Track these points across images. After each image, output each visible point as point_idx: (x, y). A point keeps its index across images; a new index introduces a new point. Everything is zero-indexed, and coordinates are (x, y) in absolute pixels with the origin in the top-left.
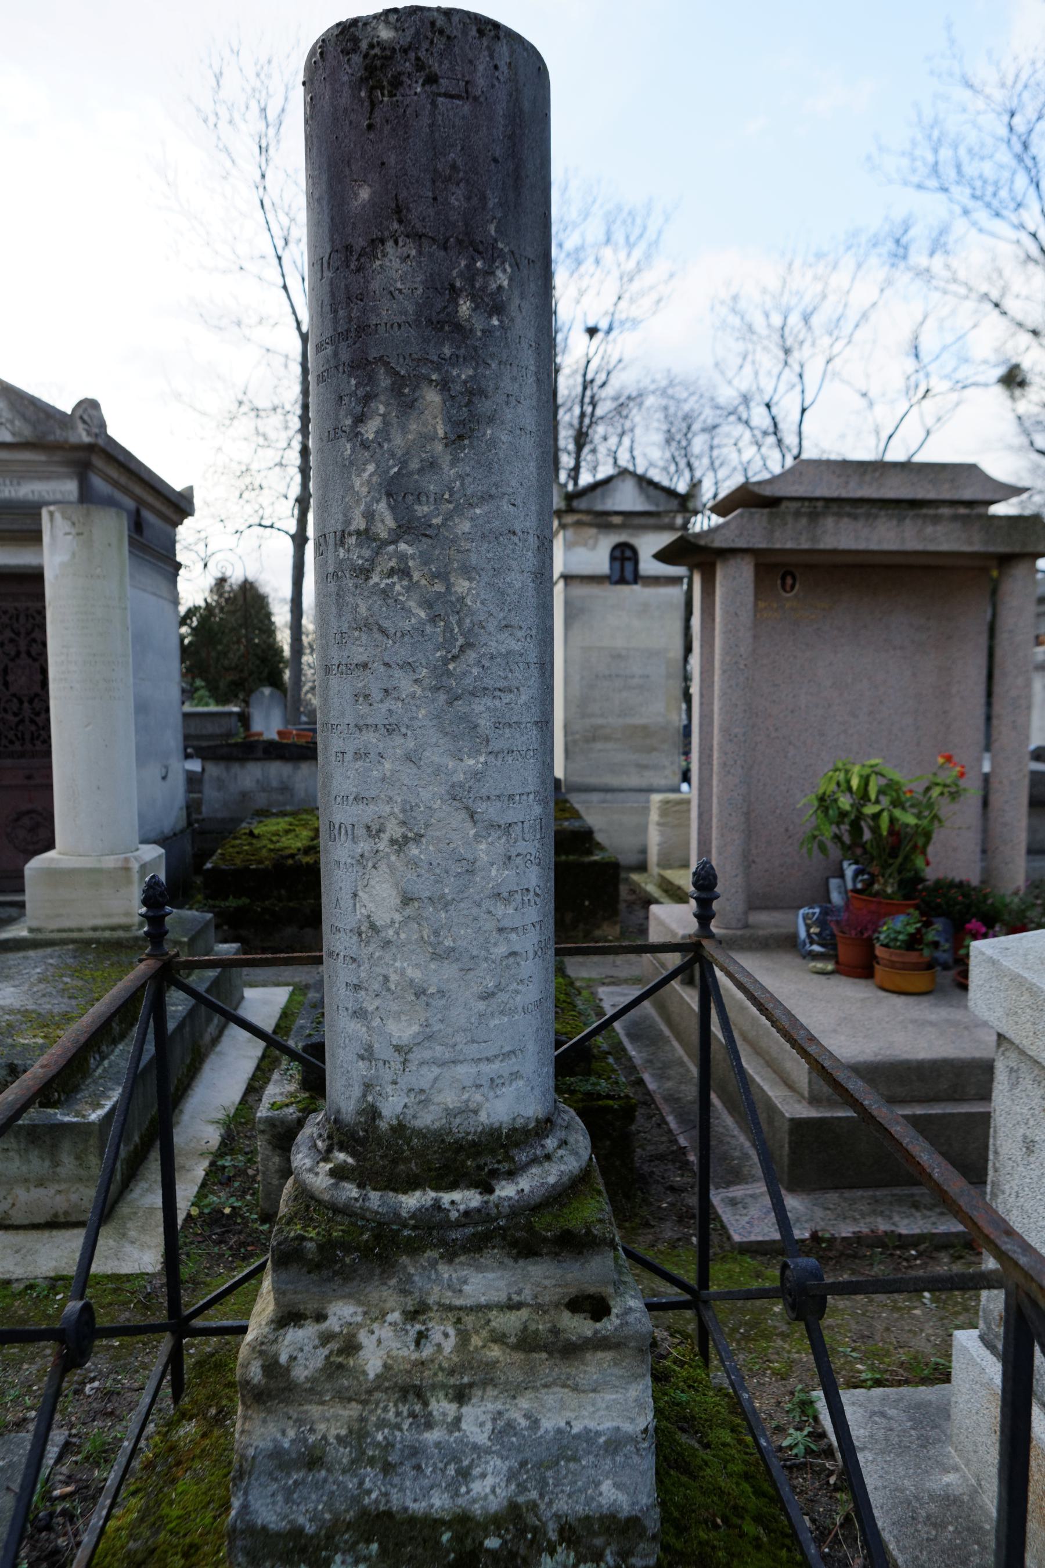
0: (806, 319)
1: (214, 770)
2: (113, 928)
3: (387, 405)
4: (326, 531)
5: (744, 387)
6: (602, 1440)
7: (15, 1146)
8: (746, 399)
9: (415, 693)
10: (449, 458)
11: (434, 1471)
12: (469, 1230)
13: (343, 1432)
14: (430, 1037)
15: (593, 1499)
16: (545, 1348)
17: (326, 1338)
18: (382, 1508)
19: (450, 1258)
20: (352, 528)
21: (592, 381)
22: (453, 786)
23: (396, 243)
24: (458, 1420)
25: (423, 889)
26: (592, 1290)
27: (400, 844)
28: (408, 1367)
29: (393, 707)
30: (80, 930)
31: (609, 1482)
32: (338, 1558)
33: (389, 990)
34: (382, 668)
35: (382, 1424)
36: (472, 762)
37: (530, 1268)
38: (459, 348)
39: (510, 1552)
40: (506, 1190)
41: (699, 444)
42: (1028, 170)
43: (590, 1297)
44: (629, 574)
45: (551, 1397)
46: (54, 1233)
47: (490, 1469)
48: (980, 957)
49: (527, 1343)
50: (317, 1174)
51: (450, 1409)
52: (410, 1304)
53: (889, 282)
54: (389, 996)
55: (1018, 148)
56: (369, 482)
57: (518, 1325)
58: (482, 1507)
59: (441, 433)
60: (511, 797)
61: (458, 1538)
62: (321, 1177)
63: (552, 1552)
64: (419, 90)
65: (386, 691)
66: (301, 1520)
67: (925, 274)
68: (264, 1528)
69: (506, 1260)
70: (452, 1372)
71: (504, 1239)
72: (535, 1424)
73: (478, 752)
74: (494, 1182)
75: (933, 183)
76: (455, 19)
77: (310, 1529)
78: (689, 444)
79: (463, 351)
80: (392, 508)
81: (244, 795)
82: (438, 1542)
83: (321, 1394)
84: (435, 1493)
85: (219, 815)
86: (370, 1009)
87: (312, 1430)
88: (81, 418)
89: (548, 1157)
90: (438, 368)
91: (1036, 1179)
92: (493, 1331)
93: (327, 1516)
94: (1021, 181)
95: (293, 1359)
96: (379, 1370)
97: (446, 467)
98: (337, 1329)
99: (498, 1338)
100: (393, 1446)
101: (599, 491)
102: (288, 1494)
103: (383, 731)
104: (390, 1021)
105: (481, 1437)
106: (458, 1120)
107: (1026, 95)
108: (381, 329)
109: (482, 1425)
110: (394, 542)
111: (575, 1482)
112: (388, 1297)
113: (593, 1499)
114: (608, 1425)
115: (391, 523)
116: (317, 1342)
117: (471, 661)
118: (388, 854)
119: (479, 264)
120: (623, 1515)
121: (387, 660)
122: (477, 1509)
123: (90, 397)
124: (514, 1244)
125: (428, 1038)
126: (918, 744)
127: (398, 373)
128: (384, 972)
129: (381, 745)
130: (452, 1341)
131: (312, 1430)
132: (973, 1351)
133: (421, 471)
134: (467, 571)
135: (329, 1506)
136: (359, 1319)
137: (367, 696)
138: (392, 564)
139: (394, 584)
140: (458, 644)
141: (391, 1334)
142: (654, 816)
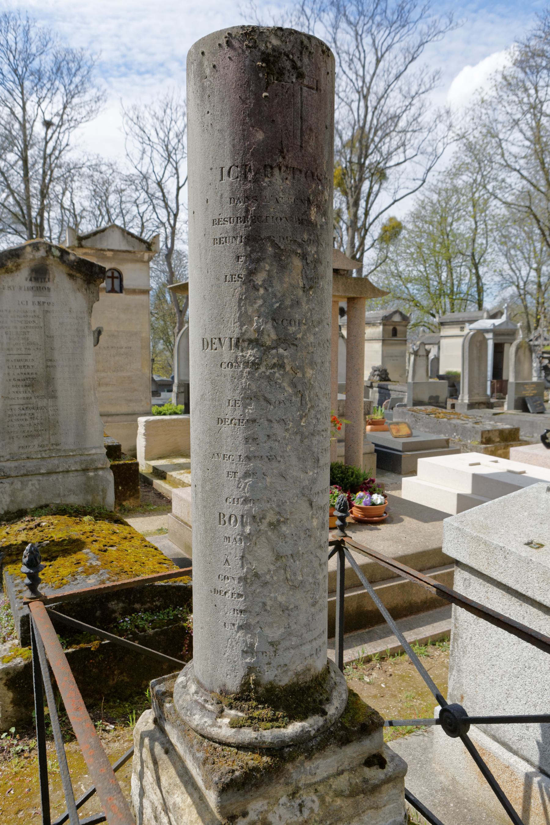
3: (271, 265)
4: (221, 336)
9: (285, 436)
10: (305, 299)
12: (318, 739)
14: (290, 634)
16: (363, 792)
19: (309, 757)
20: (246, 337)
21: (50, 155)
23: (280, 169)
25: (287, 550)
33: (266, 610)
34: (266, 423)
36: (311, 473)
38: (310, 235)
41: (113, 199)
43: (374, 756)
44: (117, 288)
49: (354, 792)
52: (290, 789)
54: (266, 614)
56: (258, 311)
59: (301, 285)
64: (294, 80)
65: (268, 436)
69: (336, 749)
71: (335, 738)
74: (323, 707)
78: (107, 198)
80: (275, 328)
86: (253, 623)
90: (300, 245)
91: (483, 631)
98: (256, 818)
99: (339, 794)
101: (98, 236)
106: (302, 677)
112: (280, 791)
115: (274, 336)
118: (266, 532)
121: (270, 417)
125: (289, 634)
127: (280, 247)
129: (264, 468)
130: (317, 803)
133: (292, 306)
134: (312, 364)
136: (266, 807)
137: (254, 439)
138: (275, 361)
139: (275, 373)
141: (285, 811)
142: (141, 430)
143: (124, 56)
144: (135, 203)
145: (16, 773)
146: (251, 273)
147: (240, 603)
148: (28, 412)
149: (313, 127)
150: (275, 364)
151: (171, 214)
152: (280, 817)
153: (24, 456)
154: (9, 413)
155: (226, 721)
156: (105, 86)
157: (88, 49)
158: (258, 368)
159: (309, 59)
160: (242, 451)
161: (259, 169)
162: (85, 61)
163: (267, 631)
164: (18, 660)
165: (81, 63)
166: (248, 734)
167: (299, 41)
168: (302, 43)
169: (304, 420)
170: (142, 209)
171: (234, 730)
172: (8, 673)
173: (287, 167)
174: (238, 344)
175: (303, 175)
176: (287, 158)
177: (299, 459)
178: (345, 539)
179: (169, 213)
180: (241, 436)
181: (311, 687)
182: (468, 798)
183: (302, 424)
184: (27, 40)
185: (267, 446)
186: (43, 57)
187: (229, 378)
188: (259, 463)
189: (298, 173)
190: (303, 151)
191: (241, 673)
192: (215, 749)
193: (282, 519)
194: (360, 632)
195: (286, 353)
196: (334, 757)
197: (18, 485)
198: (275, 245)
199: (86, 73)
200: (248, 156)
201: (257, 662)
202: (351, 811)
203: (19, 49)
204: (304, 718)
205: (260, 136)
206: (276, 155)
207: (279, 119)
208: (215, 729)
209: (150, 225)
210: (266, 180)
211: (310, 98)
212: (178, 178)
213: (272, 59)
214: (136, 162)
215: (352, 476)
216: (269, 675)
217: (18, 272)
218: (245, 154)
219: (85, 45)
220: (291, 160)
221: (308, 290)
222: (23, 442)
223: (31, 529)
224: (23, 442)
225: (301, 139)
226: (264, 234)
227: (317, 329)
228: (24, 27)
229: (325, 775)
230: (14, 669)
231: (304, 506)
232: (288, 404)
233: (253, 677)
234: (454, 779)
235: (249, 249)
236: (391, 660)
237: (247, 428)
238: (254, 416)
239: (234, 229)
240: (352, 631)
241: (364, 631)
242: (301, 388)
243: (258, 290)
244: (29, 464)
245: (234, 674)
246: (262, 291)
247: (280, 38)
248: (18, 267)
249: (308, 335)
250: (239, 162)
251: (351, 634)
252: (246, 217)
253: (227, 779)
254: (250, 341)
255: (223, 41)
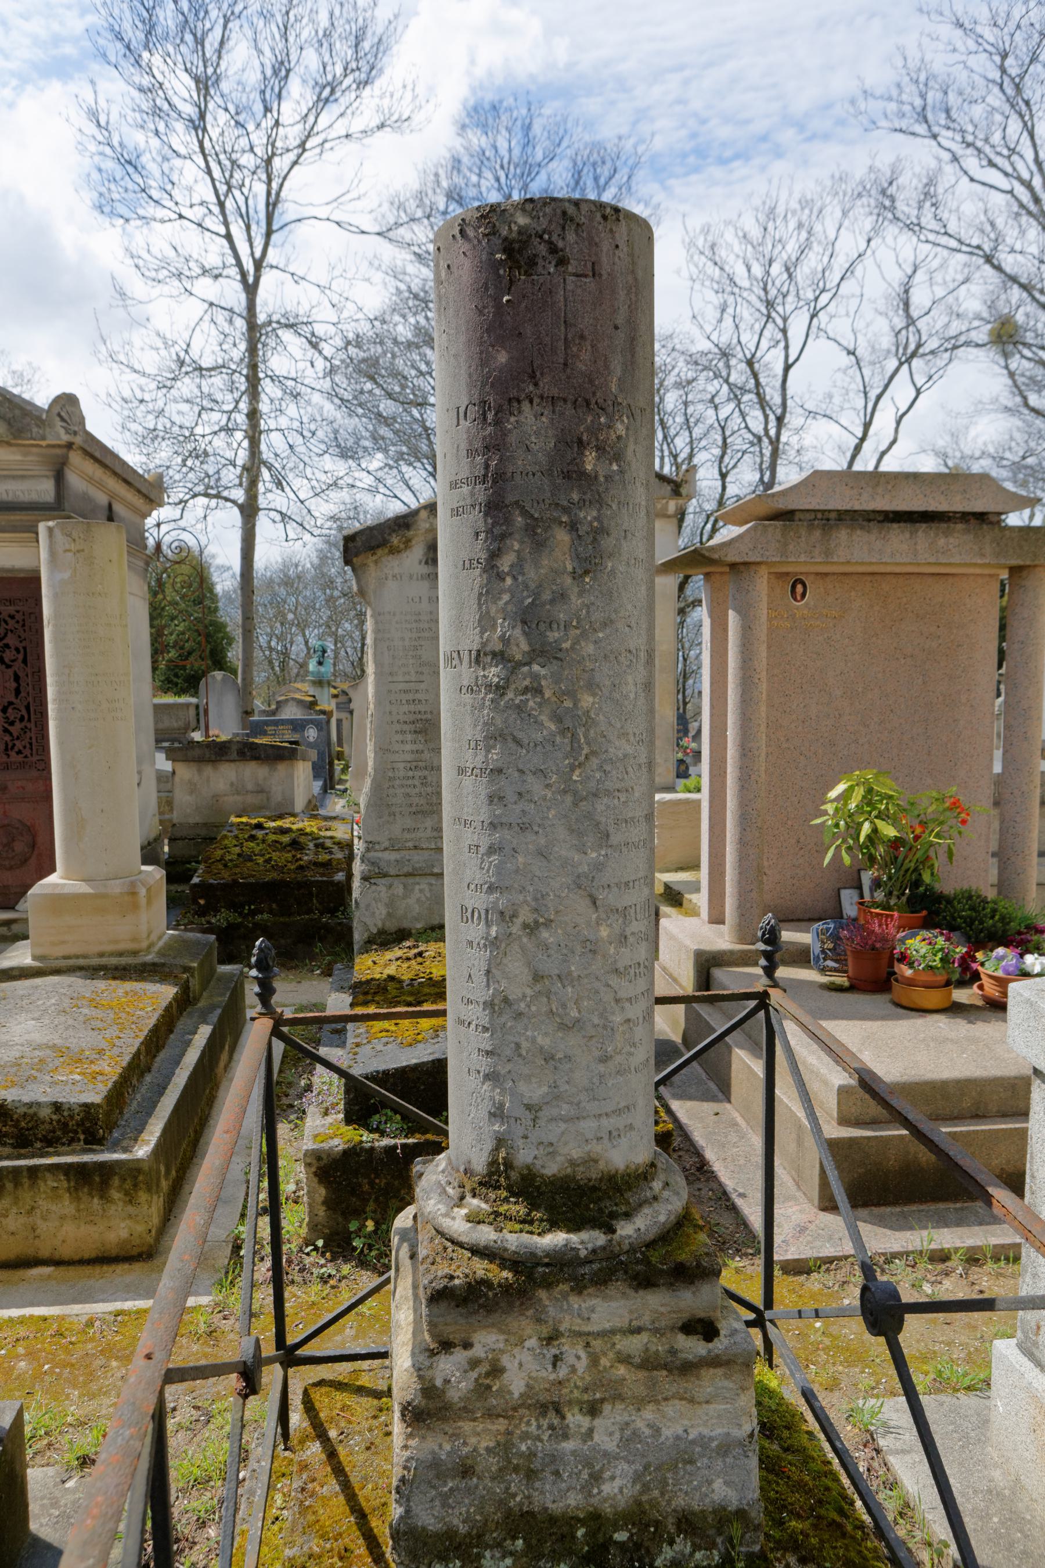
0: (789, 272)
1: (185, 772)
2: (121, 954)
3: (522, 542)
4: (460, 648)
5: (724, 340)
6: (714, 1444)
7: (65, 1184)
8: (725, 355)
10: (576, 590)
11: (570, 1476)
12: (596, 1266)
13: (492, 1444)
14: (557, 1097)
15: (706, 1495)
16: (665, 1366)
17: (474, 1363)
18: (525, 1509)
19: (579, 1289)
20: (488, 649)
22: (578, 877)
23: (531, 402)
24: (591, 1430)
25: (550, 966)
26: (702, 1315)
27: (531, 928)
28: (547, 1386)
29: (527, 809)
30: (85, 957)
31: (721, 1480)
32: (488, 1554)
33: (520, 1055)
34: (516, 774)
35: (525, 1437)
36: (594, 855)
37: (649, 1297)
38: (584, 493)
39: (635, 1544)
40: (626, 1230)
42: (1021, 116)
43: (701, 1321)
45: (671, 1409)
46: (105, 1268)
47: (618, 1473)
48: (1018, 998)
49: (648, 1363)
50: (454, 1218)
51: (585, 1421)
52: (545, 1331)
53: (876, 230)
54: (521, 1061)
55: (1010, 91)
56: (504, 610)
57: (640, 1346)
58: (611, 1506)
59: (570, 568)
60: (627, 884)
61: (591, 1534)
62: (457, 1221)
63: (671, 1543)
64: (552, 270)
66: (456, 1521)
67: (914, 227)
68: (424, 1529)
69: (628, 1291)
70: (586, 1390)
71: (626, 1272)
72: (657, 1431)
73: (601, 847)
74: (614, 1222)
75: (921, 129)
76: (584, 208)
77: (463, 1529)
79: (588, 497)
80: (524, 633)
81: (216, 797)
82: (574, 1537)
83: (473, 1412)
84: (571, 1495)
85: (191, 821)
86: (503, 1072)
87: (465, 1443)
88: (59, 415)
89: (655, 1198)
90: (566, 510)
92: (619, 1352)
93: (478, 1518)
94: (1015, 126)
95: (447, 1381)
96: (522, 1389)
97: (573, 598)
98: (483, 1355)
99: (624, 1359)
100: (535, 1455)
102: (444, 1498)
103: (517, 829)
104: (521, 1083)
105: (610, 1445)
106: (582, 1169)
107: (1019, 37)
108: (517, 477)
109: (611, 1434)
110: (528, 664)
111: (691, 1482)
112: (524, 1325)
113: (706, 1495)
114: (719, 1431)
115: (525, 647)
116: (467, 1367)
117: (595, 767)
119: (602, 420)
120: (732, 1508)
121: (521, 767)
122: (607, 1509)
123: (68, 391)
124: (635, 1277)
125: (556, 1096)
126: (929, 754)
127: (532, 516)
128: (516, 1040)
131: (465, 1443)
132: (1012, 1358)
133: (552, 602)
134: (592, 687)
135: (480, 1509)
136: (501, 1345)
137: (501, 798)
138: (527, 682)
140: (584, 752)
143: (694, 136)
144: (713, 402)
145: (313, 1303)
146: (494, 555)
147: (485, 1041)
148: (418, 774)
149: (586, 333)
150: (526, 688)
151: (772, 417)
152: (521, 1365)
153: (410, 844)
154: (390, 774)
155: (464, 1211)
156: (659, 197)
157: (630, 136)
158: (503, 694)
159: (577, 234)
160: (484, 815)
161: (501, 406)
162: (623, 158)
163: (523, 1087)
164: (336, 1141)
165: (618, 164)
166: (486, 1235)
167: (559, 211)
168: (564, 213)
169: (577, 772)
170: (724, 413)
171: (469, 1225)
172: (319, 1159)
173: (542, 397)
174: (478, 658)
175: (569, 405)
176: (541, 384)
177: (572, 831)
178: (771, 991)
179: (766, 417)
180: (483, 793)
181: (600, 1189)
182: (1034, 1517)
183: (575, 778)
184: (528, 142)
185: (518, 808)
186: (553, 165)
187: (468, 707)
188: (507, 834)
189: (561, 403)
190: (569, 371)
191: (489, 1145)
192: (445, 1248)
193: (541, 920)
194: (941, 1206)
195: (543, 672)
196: (622, 1302)
197: (399, 890)
198: (525, 513)
199: (625, 179)
200: (488, 388)
201: (508, 1132)
202: (641, 1391)
203: (515, 159)
204: (575, 1226)
205: (502, 357)
206: (524, 382)
207: (528, 330)
208: (448, 1220)
209: (739, 441)
210: (512, 419)
211: (579, 291)
212: (787, 347)
213: (516, 246)
214: (708, 328)
215: (992, 917)
216: (525, 1155)
217: (408, 552)
218: (483, 386)
219: (624, 130)
220: (547, 385)
221: (581, 576)
222: (409, 822)
223: (408, 959)
224: (409, 822)
225: (566, 354)
226: (510, 498)
227: (601, 635)
228: (523, 120)
229: (607, 1326)
230: (329, 1153)
231: (582, 905)
232: (549, 747)
233: (502, 1154)
234: (1018, 1480)
235: (490, 521)
236: (990, 1266)
237: (491, 782)
238: (499, 764)
239: (472, 494)
240: (926, 1202)
241: (952, 1205)
242: (571, 724)
243: (504, 580)
244: (416, 858)
245: (479, 1146)
246: (509, 581)
247: (529, 214)
248: (407, 543)
249: (583, 644)
250: (476, 399)
251: (922, 1207)
252: (485, 476)
253: (439, 1285)
254: (494, 654)
255: (456, 231)
